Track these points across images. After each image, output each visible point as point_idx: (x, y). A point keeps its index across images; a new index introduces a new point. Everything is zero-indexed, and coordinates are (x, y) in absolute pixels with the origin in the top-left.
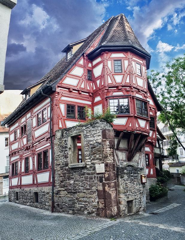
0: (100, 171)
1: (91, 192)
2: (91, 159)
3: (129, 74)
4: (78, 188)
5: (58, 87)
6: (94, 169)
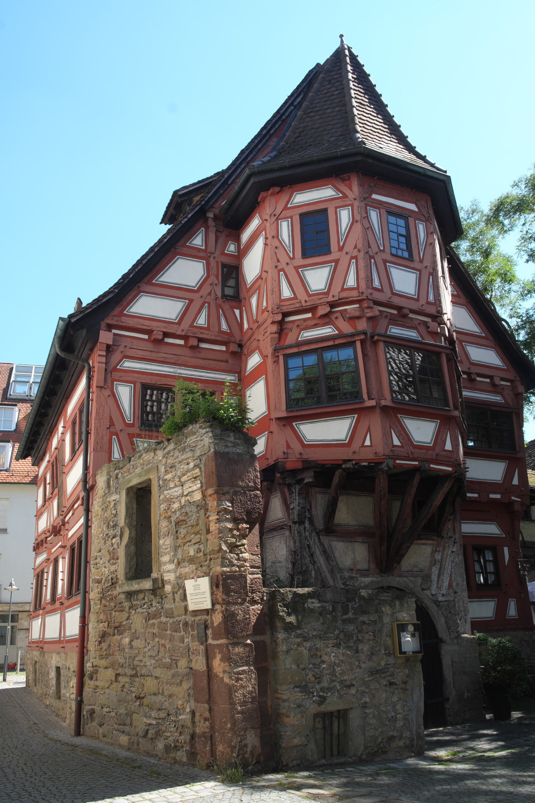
3: (356, 258)
4: (141, 661)
6: (184, 597)
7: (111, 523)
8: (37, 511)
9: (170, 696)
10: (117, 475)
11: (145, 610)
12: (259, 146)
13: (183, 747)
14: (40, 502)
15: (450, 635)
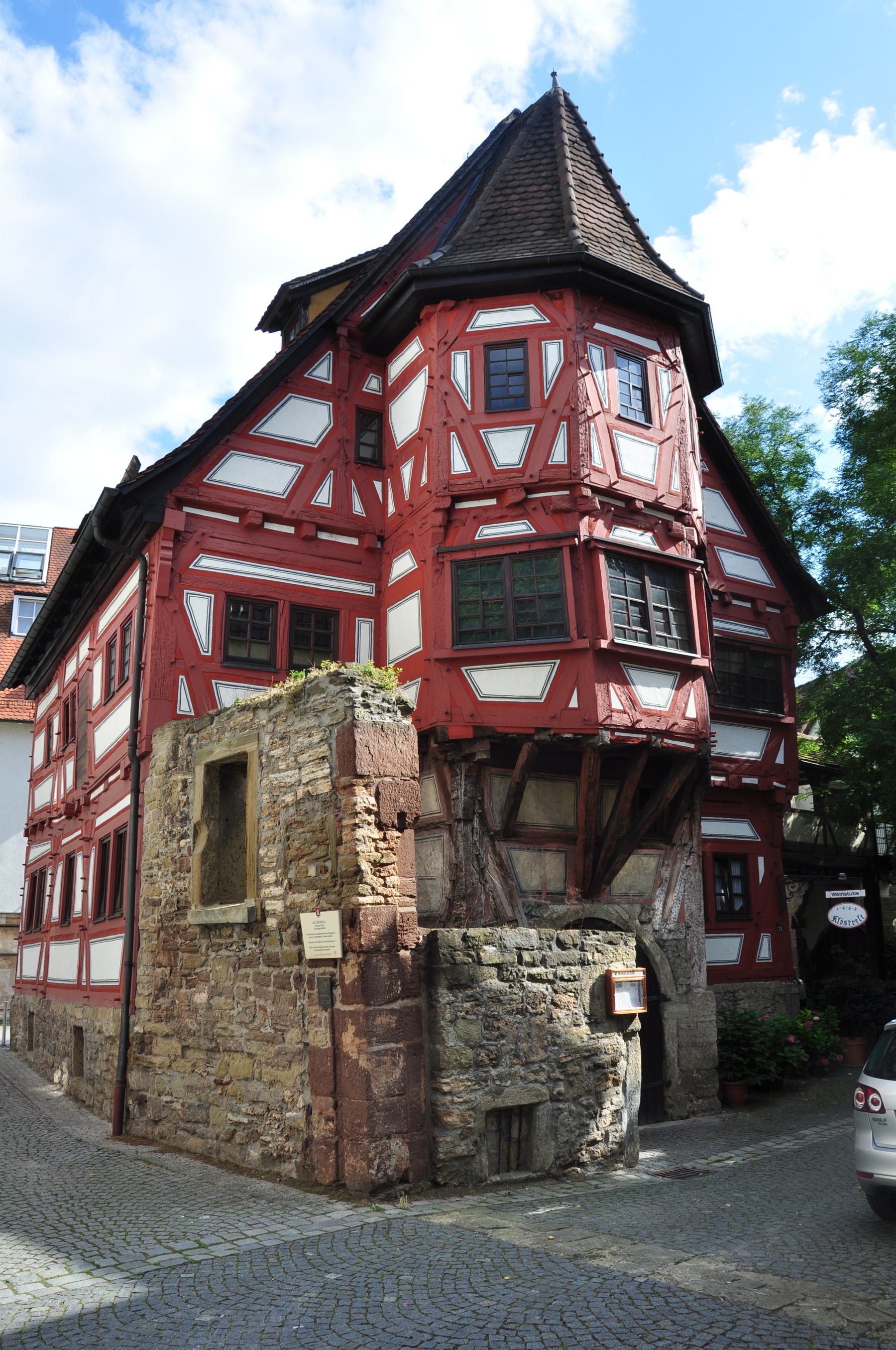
0: (320, 949)
1: (278, 1054)
4: (225, 1029)
6: (298, 939)
7: (178, 815)
9: (272, 1084)
10: (190, 740)
11: (232, 954)
13: (291, 1158)
14: (39, 759)
15: (677, 989)
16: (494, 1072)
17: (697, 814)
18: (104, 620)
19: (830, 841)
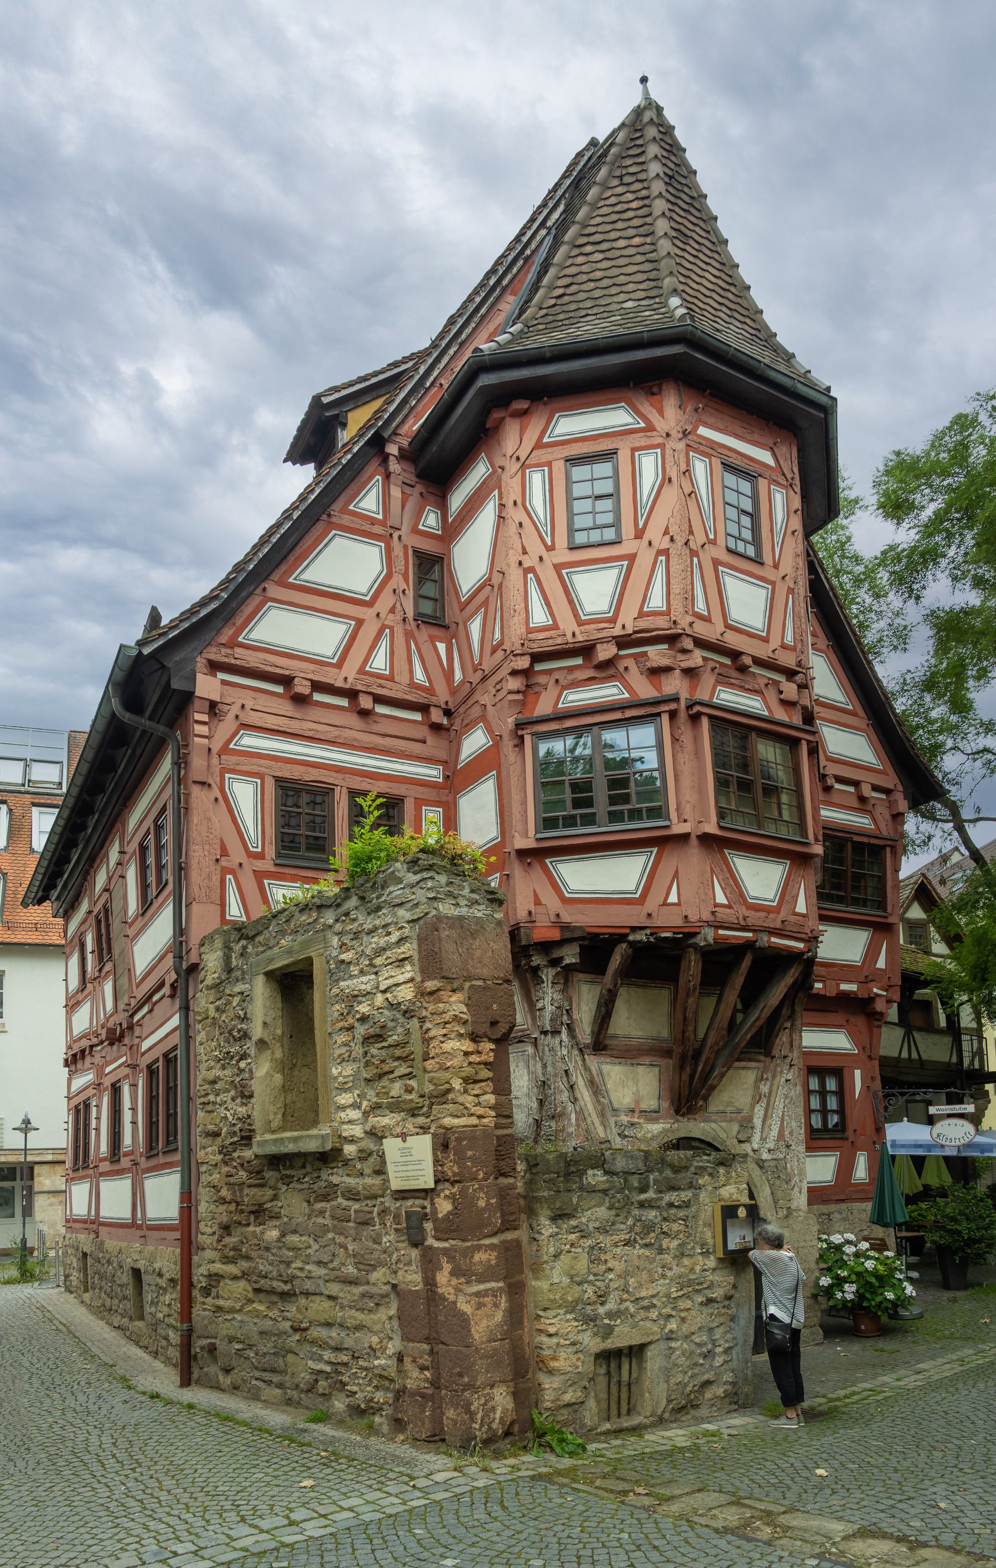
0: (408, 1178)
1: (363, 1295)
2: (365, 1104)
3: (665, 552)
4: (301, 1269)
5: (214, 667)
6: (380, 1171)
8: (68, 999)
10: (245, 948)
12: (483, 311)
13: (381, 1409)
14: (74, 983)
16: (601, 1310)
17: (798, 1022)
18: (133, 820)
19: (914, 1055)
